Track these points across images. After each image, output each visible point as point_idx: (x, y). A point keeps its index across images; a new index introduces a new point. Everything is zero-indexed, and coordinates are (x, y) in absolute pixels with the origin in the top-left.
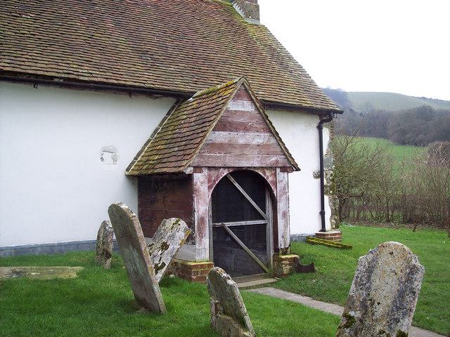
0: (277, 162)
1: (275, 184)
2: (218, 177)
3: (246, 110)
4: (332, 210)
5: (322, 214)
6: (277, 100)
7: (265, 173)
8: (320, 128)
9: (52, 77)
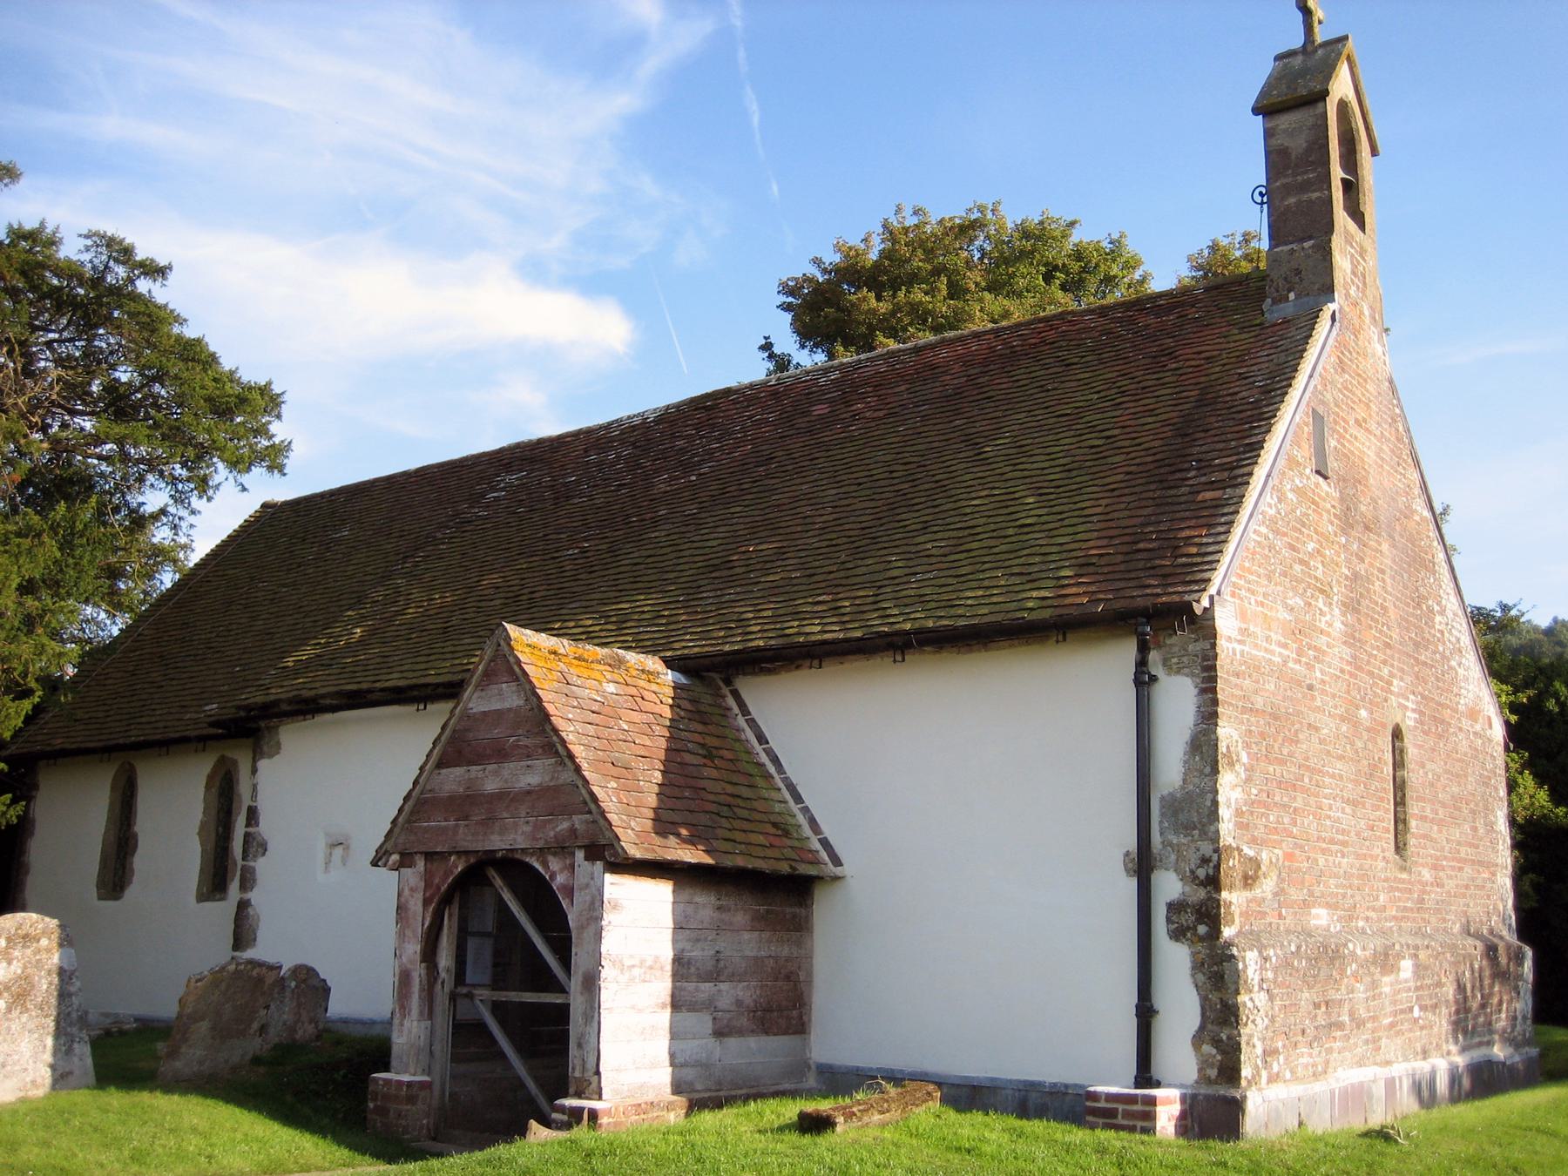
0: (573, 831)
1: (569, 891)
2: (446, 875)
3: (507, 705)
4: (1204, 1001)
5: (1146, 1013)
6: (962, 622)
7: (545, 864)
8: (1144, 681)
9: (370, 691)
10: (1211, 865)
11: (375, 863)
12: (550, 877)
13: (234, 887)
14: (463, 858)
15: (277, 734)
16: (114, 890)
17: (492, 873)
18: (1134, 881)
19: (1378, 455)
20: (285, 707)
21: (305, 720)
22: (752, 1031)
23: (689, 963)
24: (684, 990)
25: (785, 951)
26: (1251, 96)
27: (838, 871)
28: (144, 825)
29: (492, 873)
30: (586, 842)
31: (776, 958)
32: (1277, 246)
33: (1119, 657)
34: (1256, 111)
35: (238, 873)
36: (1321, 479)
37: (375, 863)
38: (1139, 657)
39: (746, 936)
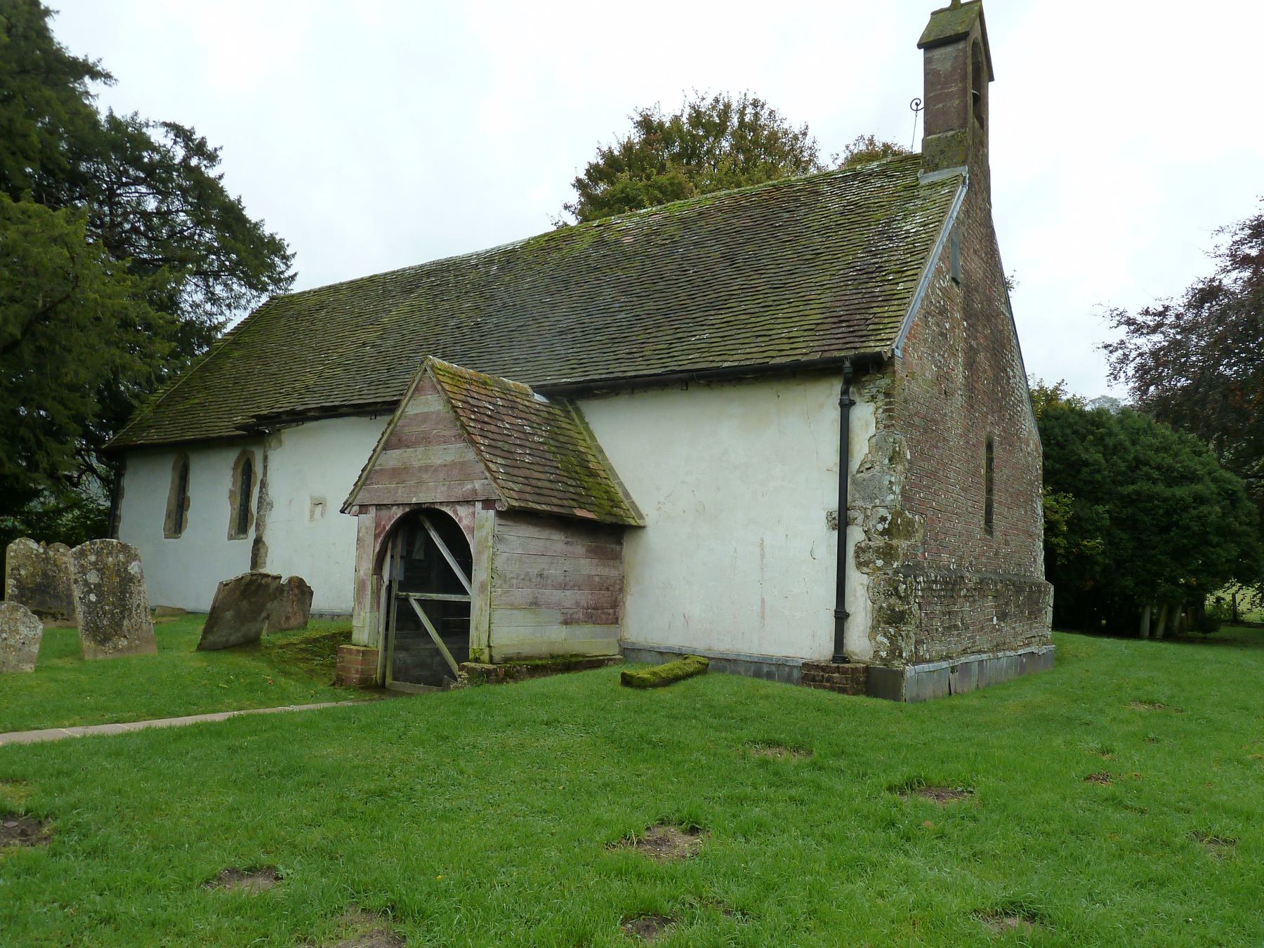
5: (841, 616)
7: (456, 512)
8: (846, 406)
10: (887, 522)
11: (342, 511)
12: (459, 520)
13: (252, 533)
14: (401, 508)
15: (280, 434)
16: (175, 532)
17: (422, 518)
18: (836, 533)
19: (984, 274)
20: (284, 417)
21: (298, 425)
22: (586, 622)
23: (547, 577)
24: (544, 594)
25: (606, 572)
26: (917, 40)
27: (641, 523)
28: (193, 492)
29: (422, 518)
30: (484, 498)
31: (601, 576)
32: (929, 135)
33: (828, 395)
34: (920, 46)
35: (255, 521)
36: (954, 284)
37: (342, 511)
38: (845, 387)
39: (583, 561)
